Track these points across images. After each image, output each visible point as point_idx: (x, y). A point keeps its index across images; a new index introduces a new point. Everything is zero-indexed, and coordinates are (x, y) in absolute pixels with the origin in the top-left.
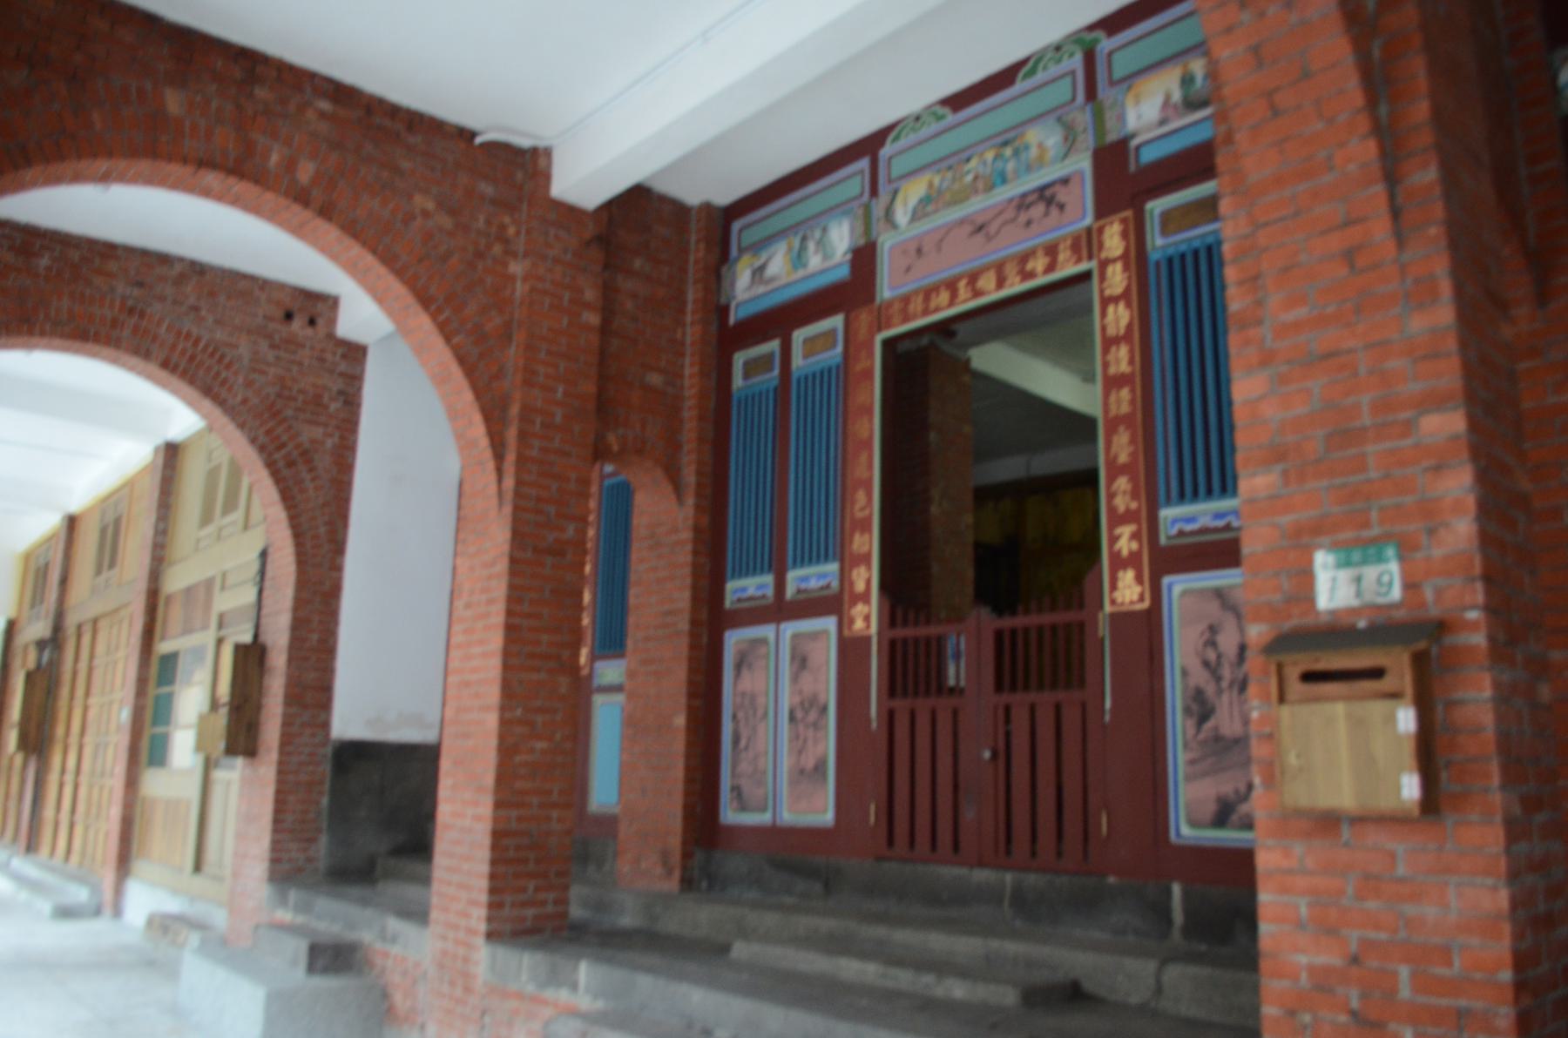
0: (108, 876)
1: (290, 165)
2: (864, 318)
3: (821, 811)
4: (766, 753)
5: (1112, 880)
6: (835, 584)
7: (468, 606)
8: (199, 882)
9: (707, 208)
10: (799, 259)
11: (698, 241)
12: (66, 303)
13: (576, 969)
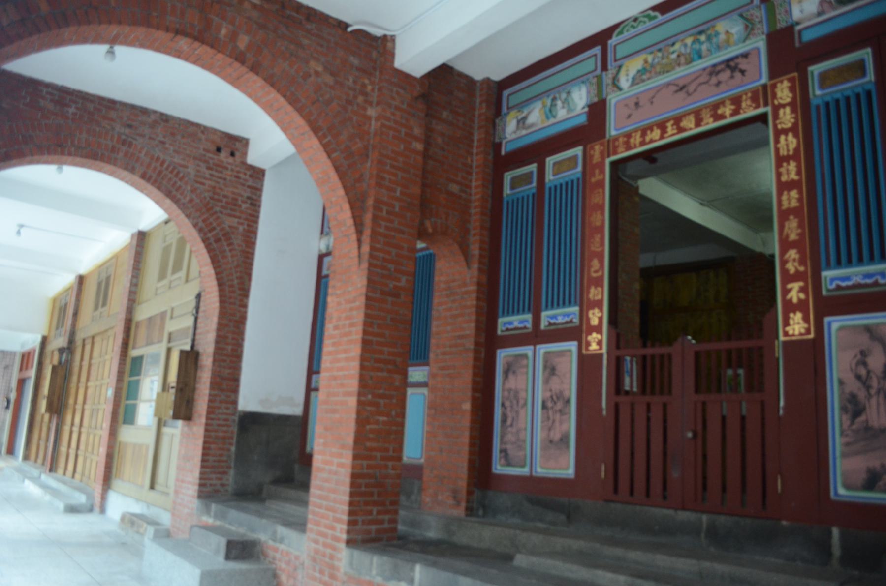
0: (97, 489)
1: (233, 37)
2: (597, 149)
3: (566, 468)
4: (525, 429)
5: (784, 523)
6: (576, 320)
7: (336, 328)
8: (152, 494)
9: (487, 81)
10: (550, 112)
11: (481, 103)
12: (84, 136)
13: (412, 570)
